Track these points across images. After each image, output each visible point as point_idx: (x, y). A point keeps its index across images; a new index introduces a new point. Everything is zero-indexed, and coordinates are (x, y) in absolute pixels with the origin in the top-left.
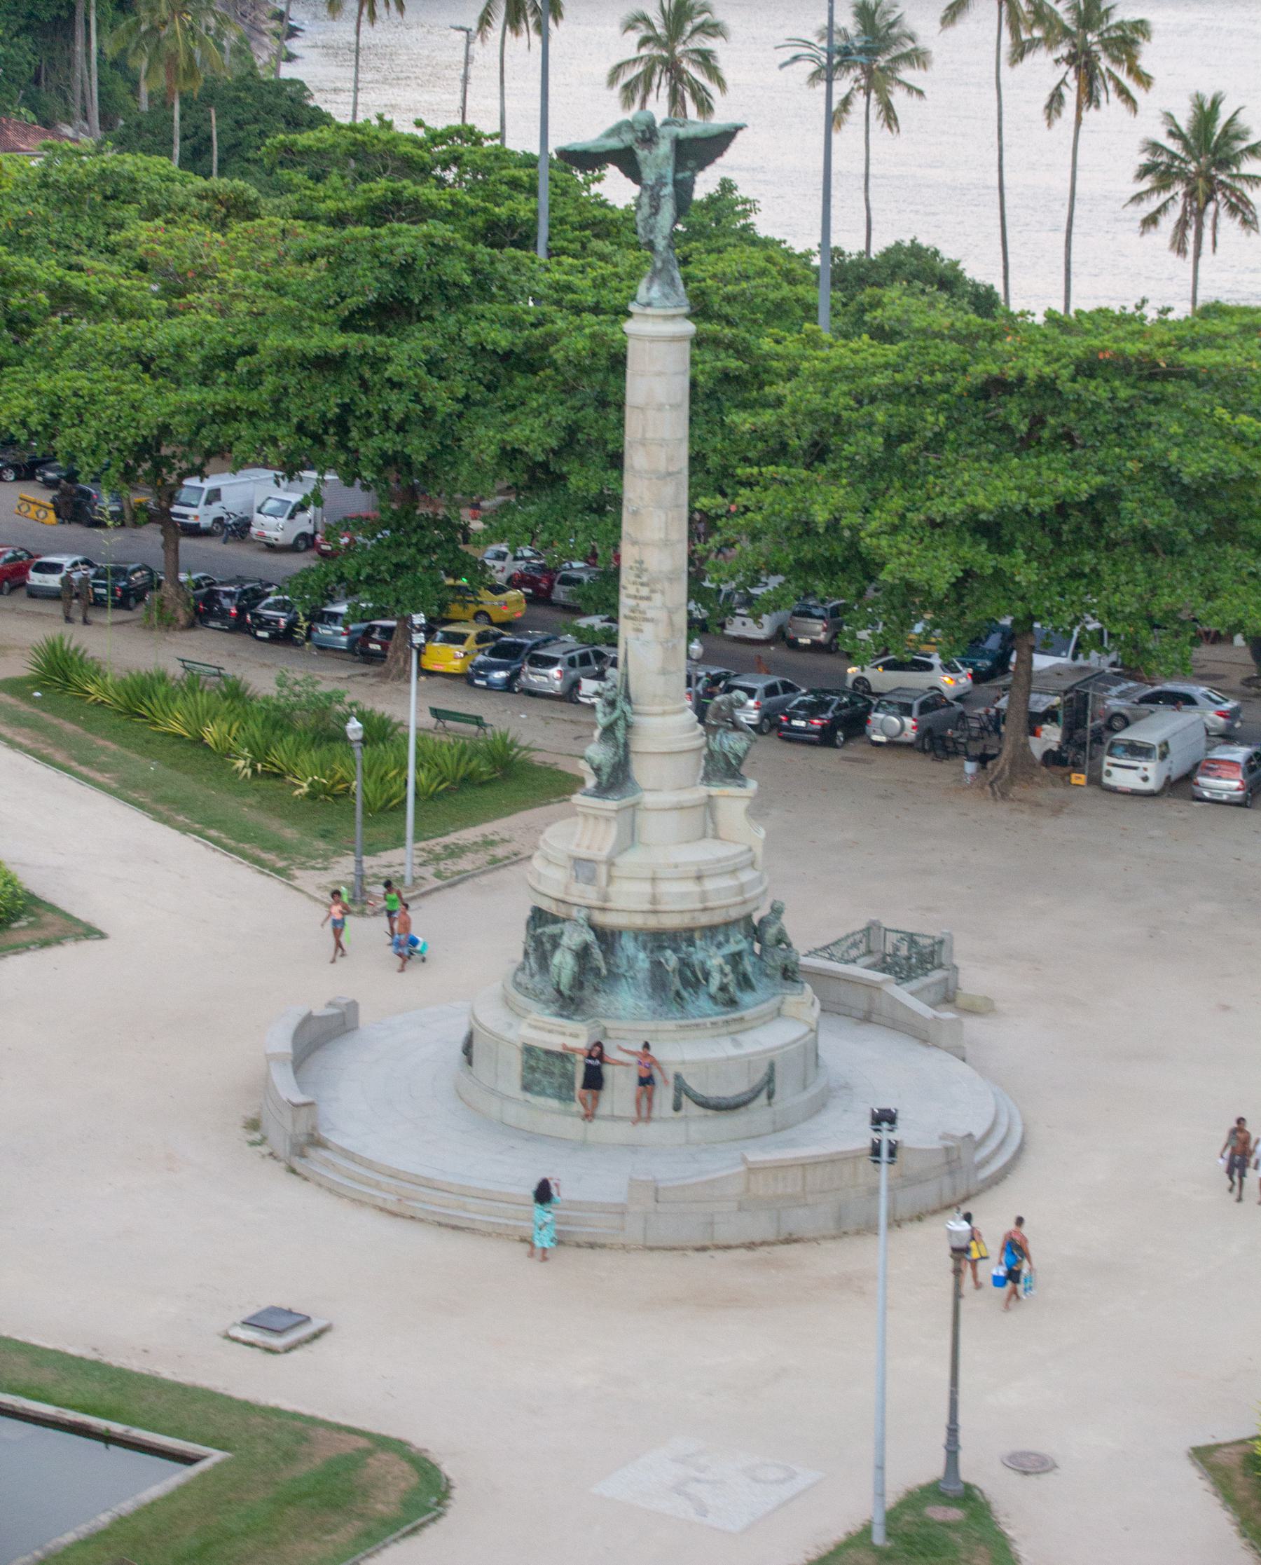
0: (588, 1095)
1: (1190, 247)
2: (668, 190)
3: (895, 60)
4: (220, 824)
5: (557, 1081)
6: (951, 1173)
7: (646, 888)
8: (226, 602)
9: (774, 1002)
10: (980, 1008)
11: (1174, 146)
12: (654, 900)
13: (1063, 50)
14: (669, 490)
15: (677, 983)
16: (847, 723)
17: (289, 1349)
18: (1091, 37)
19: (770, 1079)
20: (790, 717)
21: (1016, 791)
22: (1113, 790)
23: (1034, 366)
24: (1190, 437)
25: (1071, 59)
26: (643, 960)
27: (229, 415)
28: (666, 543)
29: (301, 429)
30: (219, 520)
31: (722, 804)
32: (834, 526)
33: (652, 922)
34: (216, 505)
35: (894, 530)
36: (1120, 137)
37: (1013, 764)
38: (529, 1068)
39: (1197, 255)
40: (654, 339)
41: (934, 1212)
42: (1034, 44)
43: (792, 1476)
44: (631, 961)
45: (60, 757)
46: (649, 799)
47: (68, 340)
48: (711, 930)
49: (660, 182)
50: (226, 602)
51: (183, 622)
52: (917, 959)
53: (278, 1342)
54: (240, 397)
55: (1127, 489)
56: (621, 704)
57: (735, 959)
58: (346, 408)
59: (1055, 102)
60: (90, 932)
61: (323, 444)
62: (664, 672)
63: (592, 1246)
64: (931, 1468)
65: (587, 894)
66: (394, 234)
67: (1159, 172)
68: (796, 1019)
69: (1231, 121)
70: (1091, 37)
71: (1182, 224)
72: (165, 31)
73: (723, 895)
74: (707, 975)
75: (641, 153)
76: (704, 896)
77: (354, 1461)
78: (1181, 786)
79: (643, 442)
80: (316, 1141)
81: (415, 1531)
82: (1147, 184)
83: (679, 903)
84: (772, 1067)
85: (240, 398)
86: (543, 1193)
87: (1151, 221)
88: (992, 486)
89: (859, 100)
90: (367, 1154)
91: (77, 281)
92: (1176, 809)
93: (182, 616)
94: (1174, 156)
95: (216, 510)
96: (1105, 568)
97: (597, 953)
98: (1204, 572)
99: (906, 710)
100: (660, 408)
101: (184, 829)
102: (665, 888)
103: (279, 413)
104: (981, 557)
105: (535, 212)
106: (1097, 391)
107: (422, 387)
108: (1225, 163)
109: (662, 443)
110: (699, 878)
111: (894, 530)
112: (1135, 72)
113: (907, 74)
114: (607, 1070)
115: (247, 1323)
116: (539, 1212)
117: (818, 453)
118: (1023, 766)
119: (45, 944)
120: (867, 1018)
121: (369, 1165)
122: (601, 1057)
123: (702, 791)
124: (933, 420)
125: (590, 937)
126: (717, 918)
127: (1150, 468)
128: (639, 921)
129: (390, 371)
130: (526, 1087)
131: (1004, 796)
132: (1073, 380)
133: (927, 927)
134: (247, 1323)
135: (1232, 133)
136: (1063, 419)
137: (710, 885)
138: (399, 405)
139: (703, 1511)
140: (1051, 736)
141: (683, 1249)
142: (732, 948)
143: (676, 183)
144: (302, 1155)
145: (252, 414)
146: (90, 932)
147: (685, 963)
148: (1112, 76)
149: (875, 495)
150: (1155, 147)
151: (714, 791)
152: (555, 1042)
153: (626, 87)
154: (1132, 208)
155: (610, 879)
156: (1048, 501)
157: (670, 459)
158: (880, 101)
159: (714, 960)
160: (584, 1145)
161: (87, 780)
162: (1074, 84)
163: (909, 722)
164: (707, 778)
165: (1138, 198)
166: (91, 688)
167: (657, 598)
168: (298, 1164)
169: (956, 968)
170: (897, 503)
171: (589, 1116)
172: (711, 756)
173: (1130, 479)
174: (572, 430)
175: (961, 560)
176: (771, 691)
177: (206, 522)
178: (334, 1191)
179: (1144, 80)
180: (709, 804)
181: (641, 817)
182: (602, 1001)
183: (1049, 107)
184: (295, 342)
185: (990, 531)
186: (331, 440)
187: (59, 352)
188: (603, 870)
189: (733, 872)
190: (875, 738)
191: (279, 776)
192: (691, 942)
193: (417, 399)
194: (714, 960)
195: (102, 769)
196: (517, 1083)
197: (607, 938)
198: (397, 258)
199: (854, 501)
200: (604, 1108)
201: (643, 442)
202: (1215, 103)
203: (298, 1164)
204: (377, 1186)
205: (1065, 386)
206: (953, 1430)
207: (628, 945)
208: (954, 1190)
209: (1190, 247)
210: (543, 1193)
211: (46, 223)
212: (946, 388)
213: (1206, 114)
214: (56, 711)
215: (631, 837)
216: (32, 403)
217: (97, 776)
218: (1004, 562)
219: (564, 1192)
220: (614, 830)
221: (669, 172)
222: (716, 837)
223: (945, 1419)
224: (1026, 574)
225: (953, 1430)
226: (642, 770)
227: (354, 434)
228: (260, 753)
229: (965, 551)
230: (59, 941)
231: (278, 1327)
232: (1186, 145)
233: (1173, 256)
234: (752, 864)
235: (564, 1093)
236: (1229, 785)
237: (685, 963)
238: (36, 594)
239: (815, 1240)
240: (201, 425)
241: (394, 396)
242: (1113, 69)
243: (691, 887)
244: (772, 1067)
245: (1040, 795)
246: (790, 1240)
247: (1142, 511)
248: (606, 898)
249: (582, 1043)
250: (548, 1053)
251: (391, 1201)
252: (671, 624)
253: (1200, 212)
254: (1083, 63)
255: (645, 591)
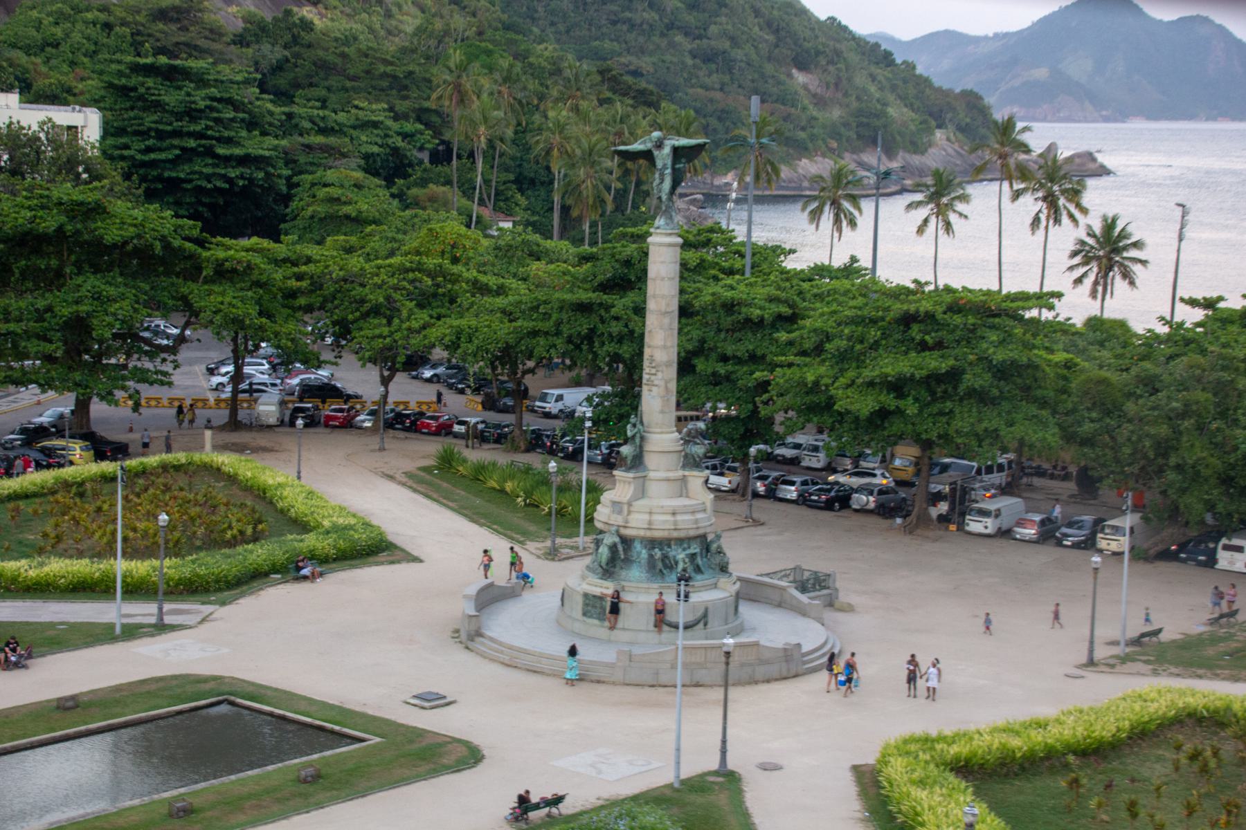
0: (612, 617)
1: (1099, 296)
2: (668, 171)
3: (953, 199)
4: (500, 524)
5: (598, 610)
6: (787, 661)
7: (646, 517)
8: (545, 440)
9: (713, 581)
10: (849, 609)
11: (1091, 241)
12: (650, 523)
13: (1040, 194)
14: (666, 321)
15: (660, 565)
16: (840, 501)
17: (432, 708)
18: (1056, 188)
19: (705, 615)
20: (811, 494)
21: (919, 531)
22: (970, 533)
23: (926, 306)
24: (1002, 342)
25: (1044, 199)
26: (644, 554)
27: (534, 333)
28: (665, 347)
29: (569, 340)
30: (561, 411)
31: (690, 479)
32: (816, 383)
33: (649, 534)
34: (560, 403)
35: (849, 386)
36: (1065, 236)
37: (918, 518)
38: (586, 605)
39: (1103, 300)
40: (661, 245)
41: (777, 680)
42: (1024, 190)
43: (650, 763)
44: (639, 553)
45: (435, 496)
46: (652, 475)
47: (472, 304)
48: (680, 541)
49: (665, 167)
50: (545, 440)
51: (523, 448)
52: (814, 583)
53: (426, 704)
54: (540, 324)
55: (968, 369)
56: (639, 426)
57: (693, 557)
58: (592, 331)
59: (1036, 222)
60: (416, 560)
61: (581, 350)
62: (662, 412)
63: (598, 682)
64: (714, 765)
65: (618, 520)
66: (623, 246)
67: (1082, 253)
68: (724, 590)
69: (1123, 229)
70: (1056, 188)
71: (1096, 283)
72: (583, 186)
73: (687, 524)
74: (677, 563)
75: (656, 153)
76: (675, 523)
77: (441, 745)
78: (1005, 533)
79: (654, 296)
80: (479, 634)
81: (458, 771)
82: (1077, 260)
83: (663, 525)
84: (706, 610)
85: (540, 325)
86: (573, 652)
87: (1078, 281)
88: (892, 365)
89: (933, 220)
90: (502, 639)
91: (483, 279)
92: (1003, 542)
93: (523, 446)
94: (1092, 247)
95: (560, 405)
96: (957, 411)
97: (620, 548)
98: (1009, 413)
99: (871, 493)
100: (663, 279)
101: (481, 525)
102: (655, 517)
103: (558, 333)
104: (890, 401)
105: (744, 266)
106: (958, 319)
107: (629, 320)
108: (1117, 251)
109: (663, 297)
110: (674, 514)
111: (849, 386)
112: (1078, 206)
113: (960, 207)
114: (622, 605)
115: (415, 697)
116: (571, 662)
117: (819, 350)
118: (924, 520)
119: (392, 562)
120: (779, 605)
121: (501, 644)
122: (618, 597)
123: (680, 473)
124: (874, 334)
125: (617, 540)
126: (682, 534)
127: (980, 359)
128: (642, 533)
129: (613, 311)
130: (584, 614)
131: (910, 533)
132: (945, 313)
133: (822, 567)
134: (415, 697)
135: (1123, 235)
136: (940, 334)
137: (679, 518)
138: (615, 328)
139: (600, 772)
140: (943, 507)
141: (643, 686)
142: (692, 551)
143: (674, 169)
144: (472, 640)
145: (546, 333)
146: (416, 560)
147: (665, 557)
148: (1065, 207)
149: (842, 371)
150: (1083, 243)
151: (687, 473)
152: (597, 591)
153: (811, 212)
154: (1068, 273)
155: (629, 513)
156: (924, 373)
157: (668, 305)
158: (944, 221)
159: (681, 555)
160: (609, 641)
161: (445, 505)
162: (1045, 211)
163: (871, 499)
164: (684, 467)
165: (1071, 268)
166: (461, 468)
167: (660, 374)
168: (470, 644)
169: (837, 590)
170: (851, 374)
171: (612, 628)
172: (686, 456)
173: (971, 364)
174: (703, 341)
175: (879, 402)
176: (804, 483)
177: (555, 411)
178: (483, 656)
179: (1084, 211)
180: (684, 479)
181: (648, 483)
182: (623, 573)
183: (1032, 224)
184: (568, 296)
185: (898, 387)
186: (585, 347)
187: (468, 309)
188: (625, 507)
189: (693, 512)
190: (855, 507)
191: (537, 507)
192: (669, 546)
193: (626, 326)
194: (681, 555)
195: (455, 501)
196: (580, 612)
197: (627, 542)
198: (623, 257)
199: (831, 373)
200: (620, 624)
201: (654, 296)
202: (1114, 220)
203: (470, 644)
204: (502, 652)
205: (939, 316)
206: (724, 742)
207: (637, 546)
208: (788, 670)
209: (1099, 296)
210: (573, 652)
211: (493, 265)
212: (883, 319)
213: (1109, 225)
214: (441, 479)
215: (642, 493)
216: (448, 331)
217: (450, 504)
218: (901, 403)
219: (585, 653)
220: (632, 488)
221: (669, 162)
222: (687, 497)
223: (720, 737)
224: (911, 409)
225: (724, 742)
226: (650, 460)
227: (596, 344)
228: (528, 494)
229: (882, 398)
230: (399, 562)
231: (432, 700)
232: (1098, 241)
233: (1090, 300)
234: (705, 510)
235: (601, 618)
236: (1030, 532)
237: (665, 557)
238: (456, 436)
239: (711, 686)
240: (522, 339)
241: (614, 323)
242: (1068, 205)
243: (669, 518)
244: (706, 610)
245: (931, 534)
246: (697, 685)
247: (974, 379)
248: (627, 522)
249: (610, 592)
250: (594, 596)
251: (506, 659)
252: (666, 388)
253: (1106, 276)
254: (1051, 200)
255: (653, 371)
